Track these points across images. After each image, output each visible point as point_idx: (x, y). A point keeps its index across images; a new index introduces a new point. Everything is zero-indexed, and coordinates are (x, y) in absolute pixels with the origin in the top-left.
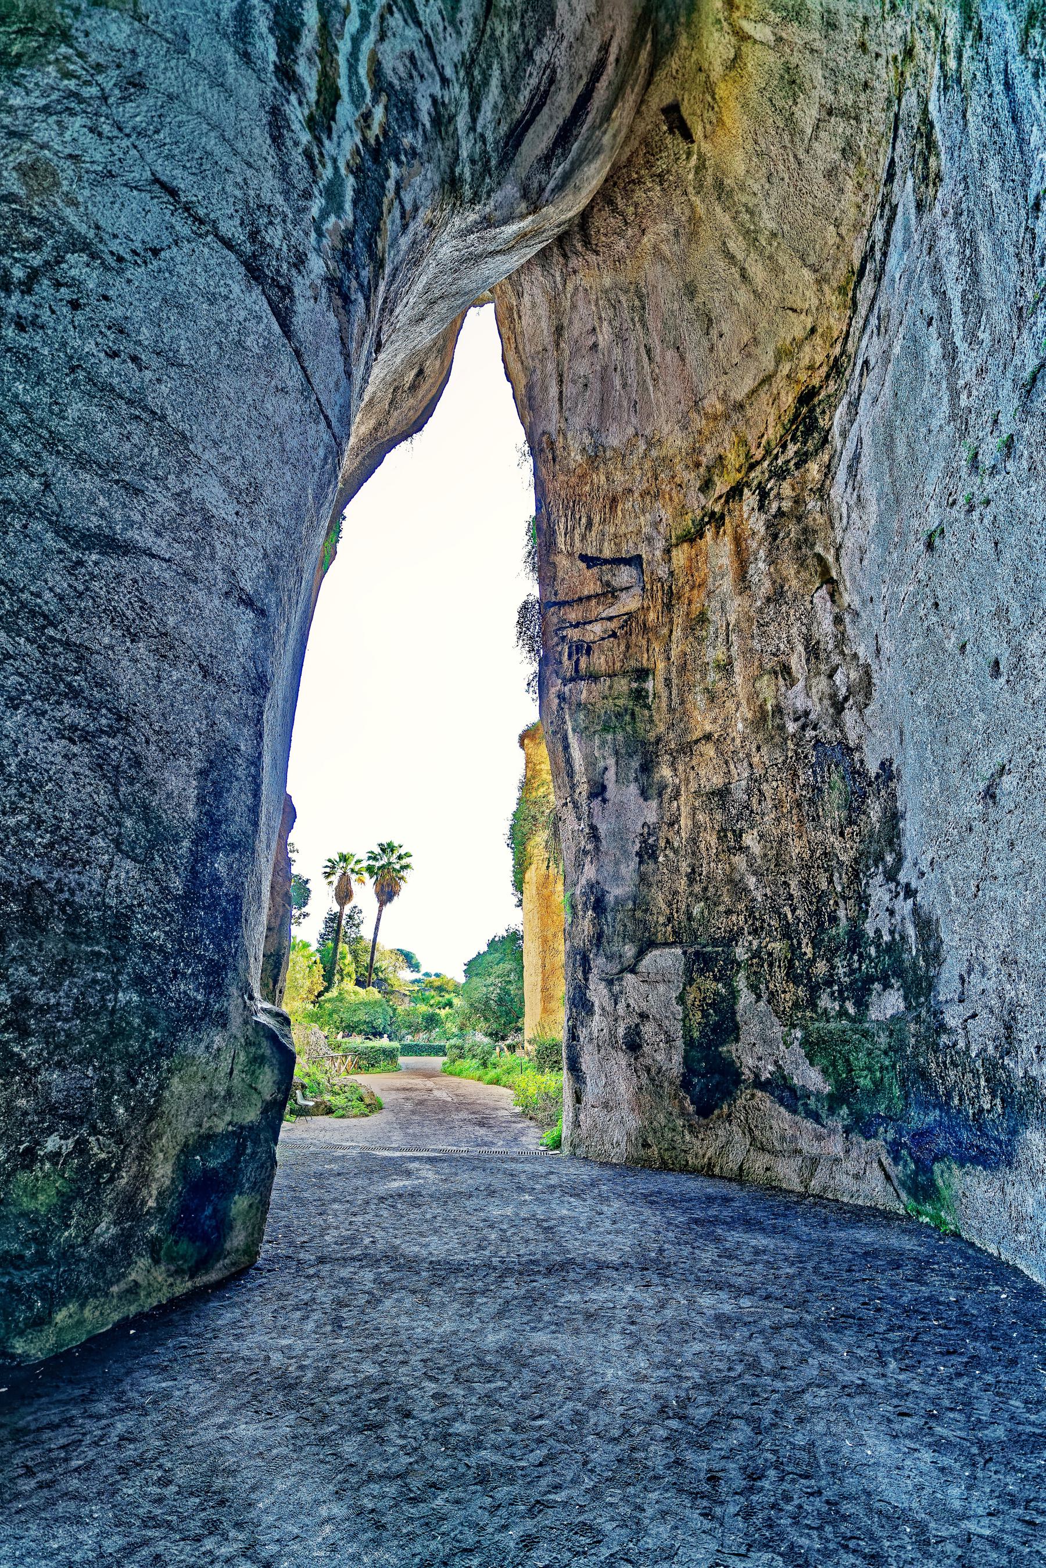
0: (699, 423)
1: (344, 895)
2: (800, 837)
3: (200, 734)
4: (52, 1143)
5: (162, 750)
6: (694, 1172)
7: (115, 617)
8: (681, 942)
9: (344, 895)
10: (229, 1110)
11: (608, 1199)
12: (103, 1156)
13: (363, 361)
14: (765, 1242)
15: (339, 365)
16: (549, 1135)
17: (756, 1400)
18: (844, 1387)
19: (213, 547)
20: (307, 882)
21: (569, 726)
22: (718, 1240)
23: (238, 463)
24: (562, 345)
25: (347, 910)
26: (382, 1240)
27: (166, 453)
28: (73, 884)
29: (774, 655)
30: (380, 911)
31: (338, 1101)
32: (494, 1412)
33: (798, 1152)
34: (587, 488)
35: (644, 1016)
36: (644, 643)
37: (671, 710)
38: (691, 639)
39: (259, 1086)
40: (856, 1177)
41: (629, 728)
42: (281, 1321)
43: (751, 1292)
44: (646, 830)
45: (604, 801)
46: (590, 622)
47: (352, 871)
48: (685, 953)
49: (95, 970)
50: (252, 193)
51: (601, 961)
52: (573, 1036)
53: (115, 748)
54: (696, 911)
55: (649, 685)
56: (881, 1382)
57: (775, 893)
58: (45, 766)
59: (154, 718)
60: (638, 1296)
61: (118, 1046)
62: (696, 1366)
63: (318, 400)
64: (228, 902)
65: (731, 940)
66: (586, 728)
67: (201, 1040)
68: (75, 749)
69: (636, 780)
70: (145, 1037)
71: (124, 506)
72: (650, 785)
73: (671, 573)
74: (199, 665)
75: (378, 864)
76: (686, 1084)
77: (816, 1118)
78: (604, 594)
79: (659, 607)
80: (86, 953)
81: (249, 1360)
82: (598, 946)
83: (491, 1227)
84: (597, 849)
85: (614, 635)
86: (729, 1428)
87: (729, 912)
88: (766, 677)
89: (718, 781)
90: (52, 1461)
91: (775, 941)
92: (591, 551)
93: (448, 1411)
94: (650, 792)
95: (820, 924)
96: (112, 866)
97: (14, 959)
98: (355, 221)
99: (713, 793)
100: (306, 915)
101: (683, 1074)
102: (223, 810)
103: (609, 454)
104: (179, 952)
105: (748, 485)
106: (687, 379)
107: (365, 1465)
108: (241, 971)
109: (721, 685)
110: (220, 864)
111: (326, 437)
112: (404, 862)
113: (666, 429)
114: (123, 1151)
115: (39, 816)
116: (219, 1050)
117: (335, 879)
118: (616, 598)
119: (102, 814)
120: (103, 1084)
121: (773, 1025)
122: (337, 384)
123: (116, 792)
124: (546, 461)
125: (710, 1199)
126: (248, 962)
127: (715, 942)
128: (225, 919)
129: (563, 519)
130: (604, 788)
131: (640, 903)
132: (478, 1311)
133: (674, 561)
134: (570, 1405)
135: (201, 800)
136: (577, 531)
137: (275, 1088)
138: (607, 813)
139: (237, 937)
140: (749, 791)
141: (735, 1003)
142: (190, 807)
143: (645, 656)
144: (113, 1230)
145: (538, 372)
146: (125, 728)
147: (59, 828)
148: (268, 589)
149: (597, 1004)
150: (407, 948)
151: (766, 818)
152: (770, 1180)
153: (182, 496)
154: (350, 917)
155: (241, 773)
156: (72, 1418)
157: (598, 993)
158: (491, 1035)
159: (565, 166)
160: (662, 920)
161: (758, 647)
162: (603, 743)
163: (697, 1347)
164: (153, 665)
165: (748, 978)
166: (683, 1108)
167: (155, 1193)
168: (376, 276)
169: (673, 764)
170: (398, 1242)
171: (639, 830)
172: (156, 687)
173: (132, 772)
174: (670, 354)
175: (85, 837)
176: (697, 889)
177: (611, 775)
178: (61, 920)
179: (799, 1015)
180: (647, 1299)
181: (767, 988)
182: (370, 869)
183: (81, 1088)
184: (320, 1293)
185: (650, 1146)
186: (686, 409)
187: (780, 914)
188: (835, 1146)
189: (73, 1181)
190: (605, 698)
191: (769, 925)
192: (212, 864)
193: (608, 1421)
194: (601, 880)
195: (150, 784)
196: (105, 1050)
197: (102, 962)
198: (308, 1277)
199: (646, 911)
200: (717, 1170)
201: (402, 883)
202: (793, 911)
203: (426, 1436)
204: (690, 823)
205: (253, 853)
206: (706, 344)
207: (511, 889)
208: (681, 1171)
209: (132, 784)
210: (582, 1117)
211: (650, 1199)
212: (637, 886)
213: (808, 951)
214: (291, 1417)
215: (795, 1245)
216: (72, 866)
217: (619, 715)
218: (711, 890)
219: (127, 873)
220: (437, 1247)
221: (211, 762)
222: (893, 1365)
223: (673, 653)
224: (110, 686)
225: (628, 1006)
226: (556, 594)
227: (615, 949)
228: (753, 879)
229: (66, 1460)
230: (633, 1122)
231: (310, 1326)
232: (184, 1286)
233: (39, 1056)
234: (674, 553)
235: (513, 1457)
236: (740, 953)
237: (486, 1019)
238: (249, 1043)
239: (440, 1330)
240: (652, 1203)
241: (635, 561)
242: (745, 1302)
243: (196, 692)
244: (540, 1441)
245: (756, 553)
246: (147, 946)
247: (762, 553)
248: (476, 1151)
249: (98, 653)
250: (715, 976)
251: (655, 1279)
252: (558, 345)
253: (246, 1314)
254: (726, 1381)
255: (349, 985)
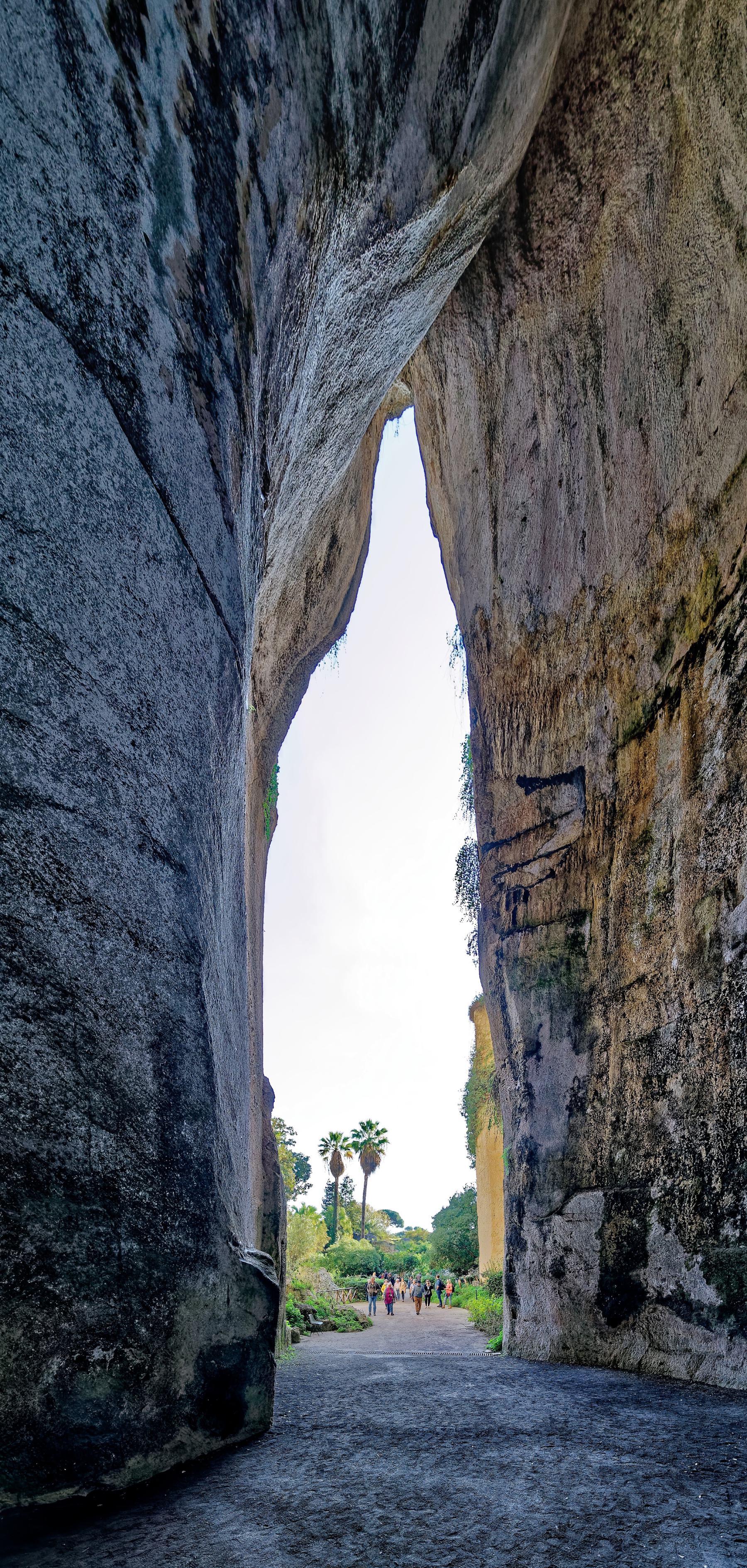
0: (661, 550)
1: (337, 1168)
2: (722, 1076)
3: (144, 1006)
4: (97, 1354)
5: (111, 1025)
6: (603, 1366)
7: (36, 882)
8: (603, 1186)
9: (337, 1168)
10: (232, 1329)
11: (531, 1386)
12: (138, 1361)
13: (247, 505)
14: (650, 1416)
15: (216, 510)
16: (493, 1342)
17: (621, 1527)
18: (694, 1520)
19: (116, 790)
20: (307, 1159)
21: (507, 985)
22: (613, 1414)
23: (123, 675)
24: (497, 456)
25: (341, 1180)
26: (359, 1414)
27: (42, 666)
28: (61, 1154)
29: (720, 871)
30: (366, 1179)
31: (338, 1321)
32: (421, 1530)
33: (688, 1351)
34: (526, 682)
35: (567, 1250)
36: (583, 879)
37: (606, 954)
38: (632, 866)
39: (253, 1311)
40: (735, 1369)
41: (564, 980)
42: (283, 1467)
43: (632, 1451)
44: (576, 1084)
45: (539, 1058)
46: (528, 862)
47: (342, 1147)
48: (605, 1195)
49: (97, 1225)
50: (57, 198)
51: (533, 1206)
52: (510, 1268)
53: (67, 1024)
54: (618, 1157)
55: (586, 929)
56: (726, 1517)
57: (693, 1134)
58: (9, 1046)
59: (98, 992)
60: (542, 1453)
61: (130, 1283)
62: (578, 1503)
63: (199, 571)
64: (200, 1165)
65: (647, 1181)
66: (523, 984)
67: (198, 1277)
68: (32, 1027)
69: (569, 1034)
70: (150, 1276)
71: (14, 745)
72: (582, 1039)
73: (616, 785)
74: (129, 932)
75: (361, 1140)
76: (599, 1301)
77: (707, 1325)
78: (543, 825)
79: (600, 833)
80: (87, 1212)
81: (257, 1491)
82: (531, 1193)
83: (441, 1405)
84: (531, 1106)
85: (552, 874)
86: (597, 1546)
87: (647, 1156)
88: (708, 900)
89: (647, 1026)
90: (124, 1549)
91: (688, 1178)
92: (530, 771)
93: (388, 1528)
94: (581, 1045)
95: (732, 1161)
96: (90, 1136)
97: (28, 1218)
98: (203, 236)
99: (642, 1040)
100: (310, 1186)
101: (598, 1295)
102: (179, 1082)
103: (551, 624)
104: (165, 1208)
105: (712, 636)
106: (648, 477)
107: (325, 1561)
108: (222, 1223)
109: (659, 917)
110: (187, 1131)
111: (218, 629)
112: (381, 1137)
113: (619, 569)
114: (152, 1358)
115: (17, 1094)
116: (214, 1284)
117: (329, 1155)
118: (554, 827)
119: (70, 1090)
120: (124, 1311)
121: (678, 1252)
122: (218, 543)
123: (78, 1068)
124: (479, 652)
125: (612, 1386)
126: (227, 1216)
127: (633, 1183)
128: (199, 1180)
129: (500, 732)
130: (538, 1045)
131: (569, 1154)
132: (421, 1462)
133: (620, 768)
134: (478, 1526)
135: (158, 1073)
136: (515, 746)
137: (266, 1313)
138: (540, 1070)
139: (213, 1195)
140: (677, 1035)
141: (646, 1236)
142: (149, 1079)
143: (583, 895)
144: (156, 1410)
145: (468, 511)
146: (72, 1004)
147: (37, 1104)
148: (183, 840)
149: (529, 1242)
150: (392, 1208)
151: (692, 1060)
152: (663, 1371)
153: (69, 724)
154: (344, 1185)
155: (189, 1044)
156: (140, 1524)
157: (530, 1233)
158: (455, 1271)
159: (489, 60)
160: (587, 1167)
161: (703, 864)
162: (539, 998)
163: (582, 1489)
164: (84, 934)
165: (660, 1213)
166: (596, 1320)
167: (183, 1385)
168: (246, 347)
169: (605, 1013)
170: (371, 1415)
171: (570, 1084)
172: (93, 959)
173: (88, 1048)
174: (632, 434)
175: (61, 1112)
176: (620, 1136)
177: (545, 1031)
178: (60, 1185)
179: (702, 1243)
180: (549, 1456)
181: (676, 1221)
182: (355, 1145)
183: (108, 1315)
184: (312, 1448)
185: (568, 1348)
186: (645, 532)
187: (694, 1153)
188: (721, 1346)
189: (121, 1379)
190: (541, 949)
191: (684, 1165)
192: (179, 1131)
193: (504, 1537)
194: (534, 1135)
195: (107, 1058)
196: (120, 1286)
197: (101, 1218)
198: (305, 1438)
199: (573, 1160)
200: (620, 1365)
201: (381, 1155)
202: (708, 1150)
203: (371, 1544)
204: (617, 1073)
205: (215, 1121)
206: (678, 405)
207: (466, 1153)
208: (592, 1366)
209: (91, 1060)
210: (517, 1329)
211: (563, 1386)
212: (567, 1138)
213: (717, 1185)
214: (280, 1528)
215: (674, 1418)
216: (56, 1138)
217: (554, 967)
218: (634, 1136)
219: (105, 1142)
220: (399, 1419)
221: (160, 1035)
222: (738, 1505)
223: (612, 886)
224: (49, 960)
225: (555, 1242)
226: (493, 833)
227: (545, 1195)
228: (674, 1123)
229: (133, 1549)
230: (556, 1332)
231: (302, 1469)
232: (217, 1444)
233: (69, 1292)
234: (620, 757)
235: (430, 1559)
236: (655, 1192)
237: (451, 1260)
238: (239, 1280)
239: (392, 1475)
240: (565, 1388)
241: (576, 776)
242: (626, 1459)
243: (132, 962)
244: (451, 1550)
245: (712, 736)
246: (137, 1204)
247: (720, 735)
248: (438, 1353)
249: (29, 925)
250: (630, 1213)
251: (558, 1442)
252: (491, 457)
253: (259, 1461)
254: (601, 1513)
255: (348, 1238)
